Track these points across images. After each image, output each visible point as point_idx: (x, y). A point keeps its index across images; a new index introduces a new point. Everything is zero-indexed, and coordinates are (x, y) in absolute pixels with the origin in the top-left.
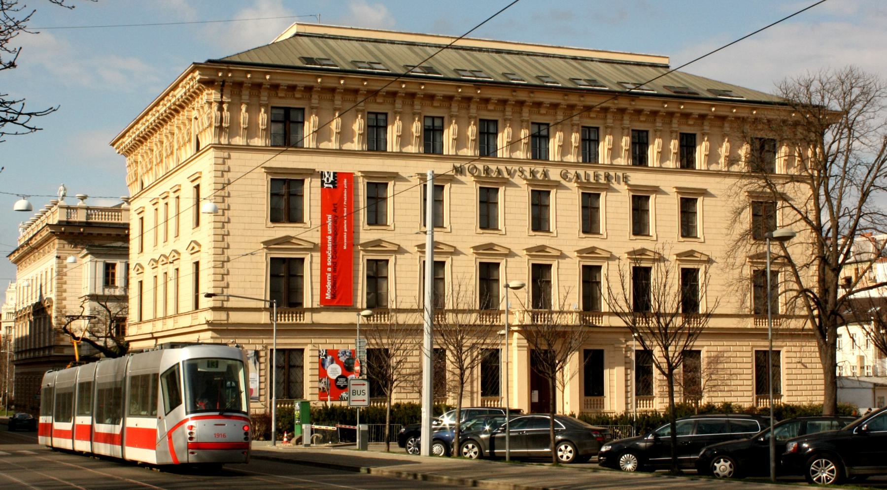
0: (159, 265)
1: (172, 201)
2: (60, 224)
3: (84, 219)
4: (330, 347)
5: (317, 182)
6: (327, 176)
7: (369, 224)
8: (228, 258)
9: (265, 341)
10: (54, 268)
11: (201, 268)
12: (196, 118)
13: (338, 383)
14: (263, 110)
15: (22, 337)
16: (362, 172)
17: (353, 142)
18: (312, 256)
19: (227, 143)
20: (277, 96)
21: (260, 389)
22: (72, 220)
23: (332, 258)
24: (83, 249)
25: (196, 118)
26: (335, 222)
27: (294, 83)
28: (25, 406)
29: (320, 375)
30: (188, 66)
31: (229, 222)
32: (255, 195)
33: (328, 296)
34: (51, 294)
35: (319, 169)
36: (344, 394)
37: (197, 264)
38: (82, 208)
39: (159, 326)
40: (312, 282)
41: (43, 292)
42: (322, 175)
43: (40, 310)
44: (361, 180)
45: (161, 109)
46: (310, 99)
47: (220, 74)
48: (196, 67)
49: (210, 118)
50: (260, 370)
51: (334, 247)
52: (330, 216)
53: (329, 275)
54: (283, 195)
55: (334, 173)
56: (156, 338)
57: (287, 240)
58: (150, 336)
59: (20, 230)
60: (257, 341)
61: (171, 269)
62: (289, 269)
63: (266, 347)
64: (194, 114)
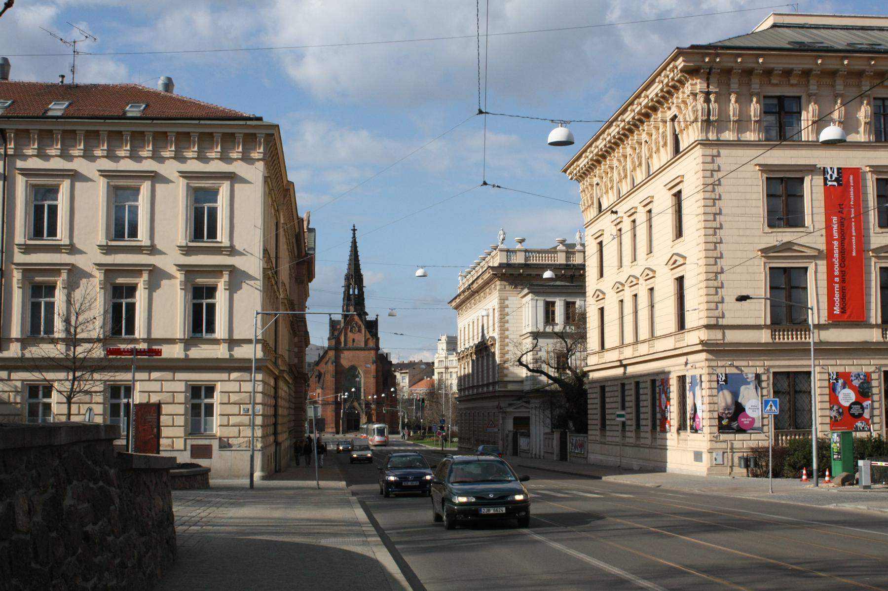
0: (626, 288)
1: (641, 217)
2: (501, 266)
3: (523, 262)
4: (841, 369)
5: (819, 180)
6: (830, 172)
7: (880, 226)
8: (722, 269)
9: (767, 363)
10: (497, 307)
11: (687, 283)
12: (598, 184)
13: (852, 411)
14: (755, 100)
15: (465, 376)
16: (870, 166)
17: (858, 133)
18: (816, 265)
19: (715, 138)
20: (770, 84)
21: (763, 418)
22: (512, 262)
23: (840, 266)
24: (523, 289)
25: (646, 141)
26: (841, 224)
27: (791, 66)
28: (469, 439)
29: (830, 402)
30: (669, 50)
31: (721, 228)
32: (749, 195)
33: (837, 311)
34: (493, 333)
35: (820, 164)
36: (859, 424)
37: (680, 280)
38: (520, 251)
39: (628, 352)
40: (817, 295)
41: (485, 332)
42: (824, 171)
43: (483, 349)
44: (869, 176)
45: (628, 116)
46: (807, 85)
47: (707, 60)
48: (680, 52)
49: (695, 111)
50: (762, 396)
51: (842, 252)
52: (835, 219)
53: (837, 286)
54: (780, 196)
55: (839, 169)
56: (625, 366)
57: (788, 246)
58: (618, 364)
59: (460, 278)
60: (758, 363)
61: (642, 291)
62: (789, 280)
63: (768, 370)
64: (596, 180)
